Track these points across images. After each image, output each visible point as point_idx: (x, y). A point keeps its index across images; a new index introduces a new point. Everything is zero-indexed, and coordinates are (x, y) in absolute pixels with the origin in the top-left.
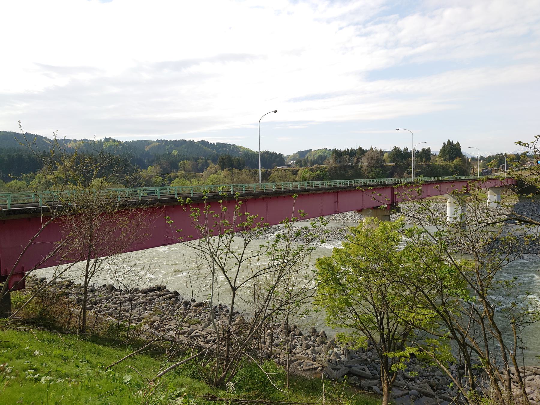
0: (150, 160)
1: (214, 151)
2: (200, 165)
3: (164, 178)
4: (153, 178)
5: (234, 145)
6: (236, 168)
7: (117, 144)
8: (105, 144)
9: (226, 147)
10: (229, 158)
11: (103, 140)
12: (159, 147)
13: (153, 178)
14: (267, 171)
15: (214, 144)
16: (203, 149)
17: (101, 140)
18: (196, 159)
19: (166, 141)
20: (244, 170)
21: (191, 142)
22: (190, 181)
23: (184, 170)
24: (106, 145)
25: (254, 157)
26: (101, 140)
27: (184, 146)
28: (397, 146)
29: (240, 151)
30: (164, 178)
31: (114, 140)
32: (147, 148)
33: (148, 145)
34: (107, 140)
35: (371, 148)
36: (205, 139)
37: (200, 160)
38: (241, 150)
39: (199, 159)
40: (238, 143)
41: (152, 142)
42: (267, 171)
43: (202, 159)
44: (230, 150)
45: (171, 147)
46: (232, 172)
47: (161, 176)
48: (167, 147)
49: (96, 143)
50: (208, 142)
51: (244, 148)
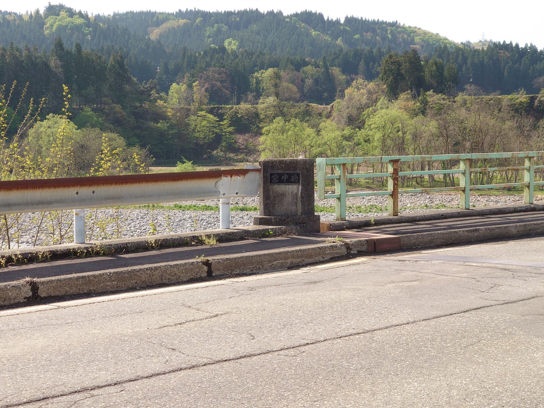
0: (171, 66)
1: (339, 41)
2: (309, 82)
3: (221, 117)
4: (193, 118)
5: (394, 25)
6: (436, 92)
7: (79, 21)
8: (49, 21)
9: (374, 31)
10: (414, 60)
11: (42, 12)
12: (186, 31)
13: (193, 118)
14: (533, 99)
15: (338, 21)
16: (308, 35)
17: (38, 12)
18: (298, 66)
19: (206, 16)
20: (460, 98)
21: (275, 18)
22: (315, 126)
23: (277, 95)
24: (52, 25)
25: (465, 59)
26: (38, 12)
27: (255, 27)
28: (282, 11)
29: (412, 42)
30: (221, 117)
31: (71, 13)
32: (154, 34)
33: (158, 24)
34: (53, 10)
35: (362, 18)
36: (314, 8)
37: (309, 69)
38: (417, 39)
39: (306, 64)
40: (407, 19)
41: (166, 17)
42: (533, 99)
43: (317, 66)
44: (384, 39)
45: (219, 30)
46: (425, 103)
47: (211, 111)
48: (209, 31)
49: (26, 18)
50: (321, 16)
51: (425, 33)
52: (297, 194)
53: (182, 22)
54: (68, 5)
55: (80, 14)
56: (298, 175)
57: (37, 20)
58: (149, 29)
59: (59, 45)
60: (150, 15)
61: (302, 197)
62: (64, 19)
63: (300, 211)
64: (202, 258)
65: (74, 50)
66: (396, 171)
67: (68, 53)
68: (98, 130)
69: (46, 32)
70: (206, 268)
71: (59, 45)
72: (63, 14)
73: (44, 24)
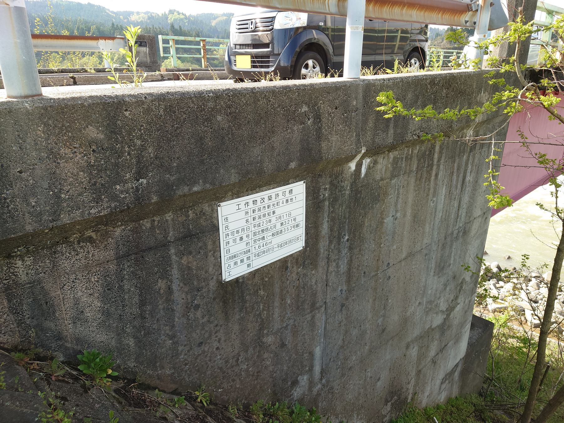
7: (182, 17)
8: (170, 16)
11: (167, 13)
32: (213, 23)
33: (215, 19)
34: (171, 12)
52: (146, 52)
53: (225, 18)
54: (177, 10)
55: (183, 14)
56: (146, 42)
57: (165, 17)
58: (211, 21)
59: (172, 26)
60: (212, 14)
61: (149, 54)
62: (176, 16)
63: (149, 61)
64: (71, 75)
65: (178, 28)
66: (204, 46)
67: (176, 30)
68: (190, 64)
69: (169, 22)
70: (72, 80)
71: (172, 26)
72: (175, 13)
73: (168, 18)
